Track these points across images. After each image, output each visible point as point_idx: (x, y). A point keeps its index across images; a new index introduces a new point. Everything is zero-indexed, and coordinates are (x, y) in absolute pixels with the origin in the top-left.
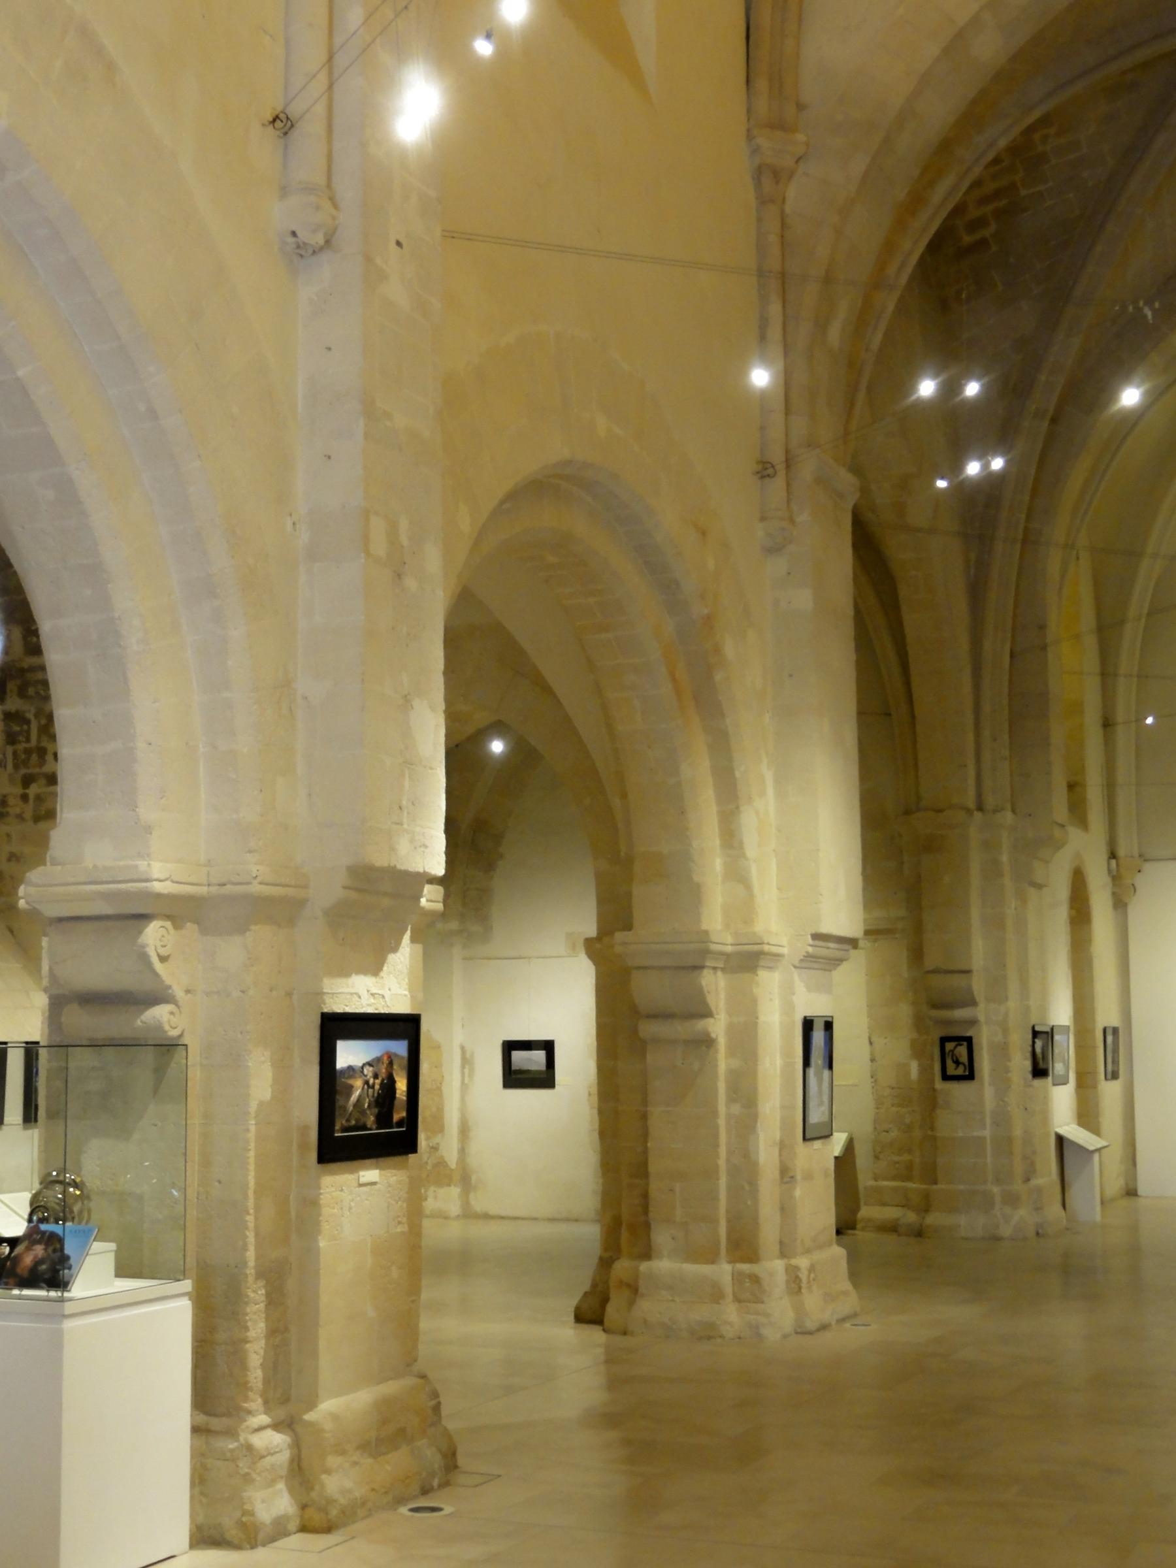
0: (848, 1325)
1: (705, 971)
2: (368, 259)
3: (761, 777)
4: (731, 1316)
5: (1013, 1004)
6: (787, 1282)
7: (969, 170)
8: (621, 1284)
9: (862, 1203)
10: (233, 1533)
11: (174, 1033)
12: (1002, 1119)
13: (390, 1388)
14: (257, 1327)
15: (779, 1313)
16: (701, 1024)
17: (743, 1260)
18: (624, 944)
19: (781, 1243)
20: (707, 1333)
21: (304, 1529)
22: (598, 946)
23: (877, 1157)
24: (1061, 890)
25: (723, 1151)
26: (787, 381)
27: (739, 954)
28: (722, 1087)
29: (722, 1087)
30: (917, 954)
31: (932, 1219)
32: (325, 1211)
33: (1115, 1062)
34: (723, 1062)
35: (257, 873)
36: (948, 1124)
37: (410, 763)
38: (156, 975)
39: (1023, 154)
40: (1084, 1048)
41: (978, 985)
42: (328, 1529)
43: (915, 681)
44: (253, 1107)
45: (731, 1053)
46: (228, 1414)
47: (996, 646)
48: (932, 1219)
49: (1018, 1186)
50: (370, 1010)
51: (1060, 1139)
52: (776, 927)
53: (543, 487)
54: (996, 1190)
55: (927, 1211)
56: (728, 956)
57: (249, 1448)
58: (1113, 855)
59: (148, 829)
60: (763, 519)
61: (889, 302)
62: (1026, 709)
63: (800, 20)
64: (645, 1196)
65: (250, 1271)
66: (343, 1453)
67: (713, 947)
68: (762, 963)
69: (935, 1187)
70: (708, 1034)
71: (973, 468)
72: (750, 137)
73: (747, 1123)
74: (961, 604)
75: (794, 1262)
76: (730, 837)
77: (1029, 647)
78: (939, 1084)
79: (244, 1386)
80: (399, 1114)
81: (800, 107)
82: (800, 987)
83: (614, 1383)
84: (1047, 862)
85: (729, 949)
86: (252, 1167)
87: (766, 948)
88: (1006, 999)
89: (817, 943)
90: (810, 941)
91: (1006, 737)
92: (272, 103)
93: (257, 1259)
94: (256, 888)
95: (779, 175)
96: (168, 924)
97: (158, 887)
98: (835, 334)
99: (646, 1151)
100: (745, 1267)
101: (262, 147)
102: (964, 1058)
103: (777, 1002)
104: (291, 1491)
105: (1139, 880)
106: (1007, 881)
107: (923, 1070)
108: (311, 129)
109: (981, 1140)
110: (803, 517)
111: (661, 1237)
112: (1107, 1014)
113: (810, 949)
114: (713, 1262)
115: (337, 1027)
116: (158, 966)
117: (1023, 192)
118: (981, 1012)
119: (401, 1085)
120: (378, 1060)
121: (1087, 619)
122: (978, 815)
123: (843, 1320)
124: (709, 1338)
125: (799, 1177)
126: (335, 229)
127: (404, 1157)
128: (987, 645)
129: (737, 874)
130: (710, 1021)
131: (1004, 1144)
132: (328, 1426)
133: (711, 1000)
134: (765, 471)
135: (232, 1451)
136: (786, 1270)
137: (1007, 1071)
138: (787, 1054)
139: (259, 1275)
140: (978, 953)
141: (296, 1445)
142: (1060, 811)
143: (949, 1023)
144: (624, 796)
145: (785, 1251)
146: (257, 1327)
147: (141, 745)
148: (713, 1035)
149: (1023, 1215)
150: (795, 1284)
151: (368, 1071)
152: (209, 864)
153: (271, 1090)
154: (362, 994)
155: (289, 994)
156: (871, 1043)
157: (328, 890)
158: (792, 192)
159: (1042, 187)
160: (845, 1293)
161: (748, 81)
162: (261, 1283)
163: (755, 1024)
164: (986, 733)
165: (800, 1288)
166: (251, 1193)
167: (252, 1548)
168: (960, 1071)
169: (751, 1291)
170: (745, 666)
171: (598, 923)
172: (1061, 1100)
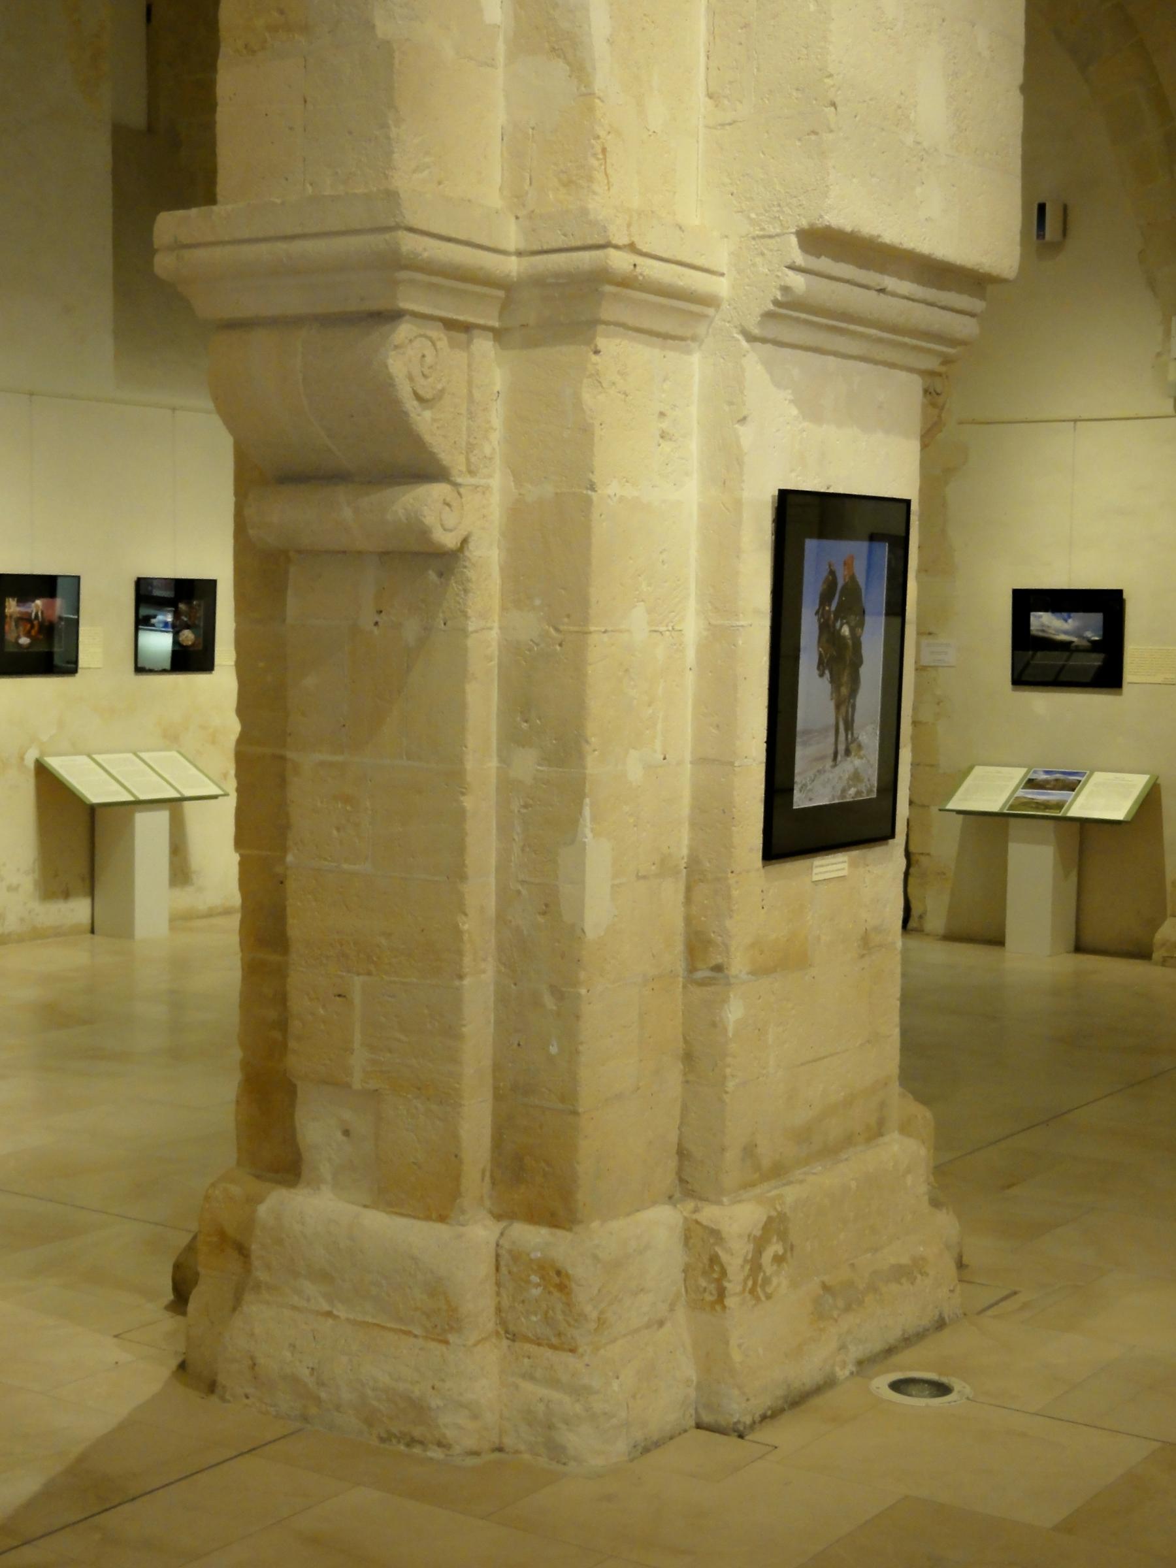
1: (404, 330)
4: (478, 1386)
15: (638, 1372)
16: (428, 504)
18: (179, 246)
19: (682, 1153)
20: (399, 1434)
34: (487, 619)
45: (518, 593)
52: (689, 198)
56: (508, 288)
68: (608, 311)
73: (551, 815)
75: (709, 1214)
85: (512, 267)
87: (620, 261)
89: (824, 264)
90: (799, 258)
100: (532, 1237)
103: (694, 446)
113: (798, 281)
114: (442, 1219)
124: (412, 1442)
125: (738, 965)
130: (438, 490)
136: (687, 1239)
138: (720, 601)
145: (689, 1178)
150: (706, 1276)
165: (721, 1294)
169: (544, 1310)
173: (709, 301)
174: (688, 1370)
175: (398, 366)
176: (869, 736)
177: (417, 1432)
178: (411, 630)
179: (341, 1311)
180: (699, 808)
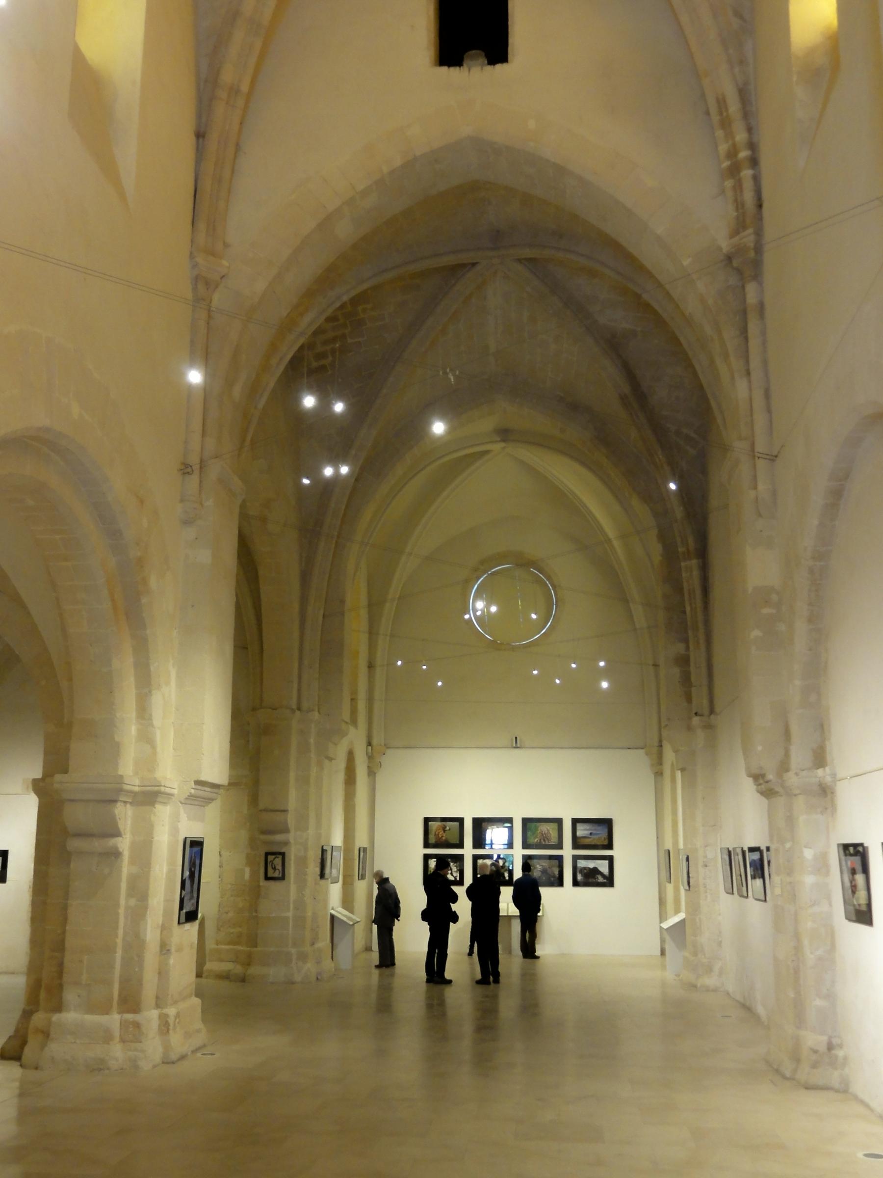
0: (199, 1055)
1: (119, 804)
4: (117, 1053)
5: (311, 831)
6: (159, 1026)
9: (207, 959)
12: (300, 905)
15: (153, 1048)
16: (112, 842)
17: (128, 1011)
19: (157, 998)
20: (98, 1067)
22: (41, 784)
23: (219, 930)
25: (121, 932)
28: (124, 886)
29: (124, 886)
30: (254, 799)
31: (254, 970)
33: (364, 868)
34: (126, 868)
40: (348, 861)
41: (291, 820)
43: (264, 626)
45: (132, 862)
48: (254, 970)
51: (333, 917)
52: (170, 775)
55: (249, 964)
56: (135, 794)
58: (369, 744)
60: (182, 501)
62: (331, 650)
63: (229, 191)
64: (61, 965)
68: (159, 799)
69: (255, 949)
70: (116, 848)
71: (328, 471)
72: (192, 256)
73: (139, 913)
75: (165, 1011)
77: (334, 612)
78: (263, 882)
81: (226, 245)
82: (183, 816)
83: (24, 1115)
84: (336, 744)
85: (136, 789)
87: (163, 789)
88: (307, 828)
91: (317, 665)
98: (237, 391)
99: (64, 932)
100: (129, 1017)
107: (254, 874)
110: (209, 503)
111: (70, 996)
112: (361, 840)
113: (193, 791)
114: (107, 1014)
117: (350, 341)
118: (291, 837)
121: (363, 600)
122: (298, 713)
124: (100, 1070)
125: (173, 949)
129: (146, 737)
130: (120, 839)
131: (300, 921)
133: (121, 825)
134: (186, 469)
137: (305, 874)
140: (293, 801)
142: (346, 715)
144: (70, 679)
145: (159, 1003)
148: (121, 850)
149: (310, 967)
150: (165, 1027)
156: (220, 855)
159: (360, 339)
160: (199, 1031)
161: (193, 222)
163: (151, 842)
165: (168, 1030)
168: (276, 874)
169: (133, 1033)
170: (164, 596)
171: (44, 767)
172: (335, 891)
173: (172, 795)
174: (160, 1050)
175: (117, 812)
176: (195, 895)
177: (102, 1067)
178: (106, 871)
179: (78, 1041)
180: (165, 910)
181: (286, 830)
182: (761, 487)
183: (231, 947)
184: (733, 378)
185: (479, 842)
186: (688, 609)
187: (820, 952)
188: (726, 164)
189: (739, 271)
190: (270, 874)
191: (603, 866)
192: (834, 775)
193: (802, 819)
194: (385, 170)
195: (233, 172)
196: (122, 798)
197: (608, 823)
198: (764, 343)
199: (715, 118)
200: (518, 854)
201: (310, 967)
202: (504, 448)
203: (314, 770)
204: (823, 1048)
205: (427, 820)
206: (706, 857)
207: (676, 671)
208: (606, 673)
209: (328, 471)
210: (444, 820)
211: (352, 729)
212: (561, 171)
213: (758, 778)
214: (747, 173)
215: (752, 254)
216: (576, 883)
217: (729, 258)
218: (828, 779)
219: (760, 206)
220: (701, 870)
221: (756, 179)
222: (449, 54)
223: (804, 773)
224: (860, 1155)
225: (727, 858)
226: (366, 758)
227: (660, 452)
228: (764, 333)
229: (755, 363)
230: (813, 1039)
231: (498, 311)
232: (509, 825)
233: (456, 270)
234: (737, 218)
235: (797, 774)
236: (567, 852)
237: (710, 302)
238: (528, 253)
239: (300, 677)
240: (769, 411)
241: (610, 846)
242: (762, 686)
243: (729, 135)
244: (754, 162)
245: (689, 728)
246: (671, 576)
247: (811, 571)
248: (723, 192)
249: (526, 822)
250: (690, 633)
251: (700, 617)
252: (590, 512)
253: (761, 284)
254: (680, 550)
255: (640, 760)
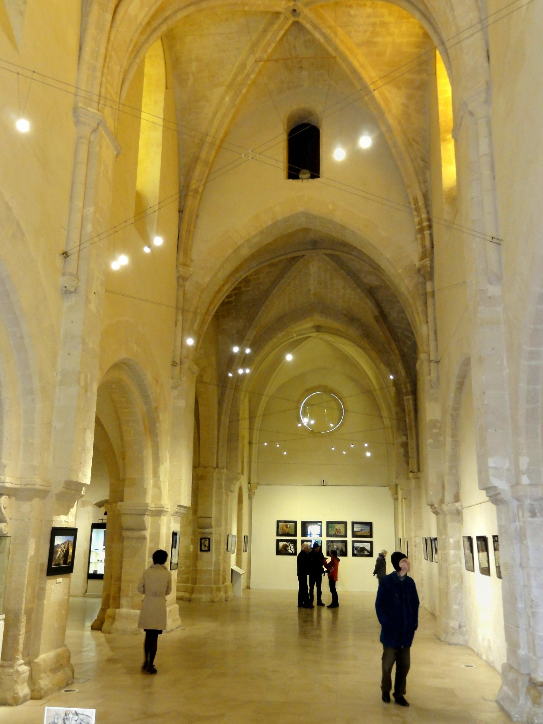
1: (146, 516)
2: (87, 297)
3: (166, 455)
5: (223, 528)
7: (233, 284)
8: (109, 617)
10: (10, 701)
11: (5, 532)
12: (217, 564)
13: (60, 650)
14: (23, 631)
21: (32, 699)
24: (236, 494)
26: (197, 342)
27: (156, 511)
31: (194, 596)
32: (47, 591)
33: (246, 546)
35: (38, 482)
36: (201, 565)
37: (84, 449)
38: (2, 513)
39: (246, 281)
40: (239, 542)
41: (213, 522)
42: (40, 698)
44: (29, 557)
45: (151, 541)
46: (11, 660)
47: (225, 419)
48: (194, 596)
49: (221, 585)
50: (64, 526)
51: (232, 570)
53: (117, 366)
54: (214, 586)
56: (152, 511)
57: (17, 671)
58: (249, 483)
59: (5, 466)
61: (210, 319)
62: (232, 439)
65: (23, 612)
66: (46, 672)
67: (149, 508)
70: (145, 536)
71: (241, 371)
72: (177, 266)
74: (216, 406)
76: (156, 474)
77: (234, 419)
78: (199, 553)
79: (17, 651)
80: (69, 560)
81: (192, 260)
82: (172, 522)
85: (153, 509)
86: (26, 577)
87: (164, 509)
88: (221, 526)
92: (62, 248)
93: (26, 607)
94: (37, 487)
95: (184, 279)
96: (7, 497)
97: (8, 485)
99: (121, 573)
101: (59, 260)
102: (207, 545)
104: (28, 685)
105: (256, 491)
106: (224, 490)
107: (195, 548)
108: (73, 257)
109: (211, 571)
110: (184, 379)
112: (245, 533)
115: (57, 531)
116: (3, 510)
118: (213, 530)
119: (71, 551)
120: (65, 542)
123: (177, 628)
126: (77, 287)
127: (68, 575)
128: (223, 418)
129: (157, 486)
131: (217, 572)
132: (42, 663)
133: (146, 525)
134: (174, 364)
135: (12, 672)
138: (167, 542)
139: (25, 613)
141: (31, 671)
142: (240, 471)
143: (203, 533)
144: (124, 459)
146: (23, 631)
147: (5, 439)
151: (62, 546)
152: (21, 478)
153: (35, 552)
154: (63, 521)
155: (42, 521)
157: (58, 488)
158: (187, 284)
160: (178, 619)
162: (25, 616)
164: (220, 444)
166: (25, 585)
167: (17, 705)
168: (206, 549)
170: (165, 421)
172: (233, 557)
181: (211, 527)
182: (432, 375)
183: (183, 584)
184: (421, 324)
185: (304, 534)
186: (407, 420)
187: (456, 585)
188: (418, 227)
189: (424, 276)
190: (203, 548)
191: (367, 546)
192: (462, 506)
193: (449, 525)
194: (264, 226)
195: (195, 227)
196: (147, 513)
197: (370, 524)
198: (434, 309)
199: (413, 206)
200: (324, 539)
201: (222, 594)
202: (318, 335)
203: (224, 497)
204: (457, 627)
205: (278, 522)
206: (415, 542)
207: (402, 450)
208: (368, 449)
209: (241, 371)
210: (285, 522)
211: (242, 476)
212: (343, 227)
213: (432, 506)
214: (427, 232)
215: (429, 269)
216: (354, 555)
217: (419, 270)
218: (460, 508)
219: (433, 247)
220: (414, 548)
221: (431, 235)
222: (293, 174)
223: (450, 505)
224: (463, 666)
225: (425, 542)
226: (248, 490)
227: (393, 344)
228: (434, 305)
229: (430, 318)
230: (453, 624)
231: (316, 277)
232: (320, 524)
233: (295, 259)
234: (423, 252)
235: (447, 505)
236: (349, 539)
237: (410, 289)
238: (329, 252)
239: (218, 451)
240: (436, 340)
241: (371, 536)
242: (434, 465)
243: (419, 215)
244: (430, 227)
245: (408, 478)
246: (400, 403)
247: (452, 415)
248: (417, 239)
249: (328, 523)
250: (408, 432)
251: (413, 424)
252: (361, 367)
253: (433, 282)
254: (404, 390)
255: (386, 492)
